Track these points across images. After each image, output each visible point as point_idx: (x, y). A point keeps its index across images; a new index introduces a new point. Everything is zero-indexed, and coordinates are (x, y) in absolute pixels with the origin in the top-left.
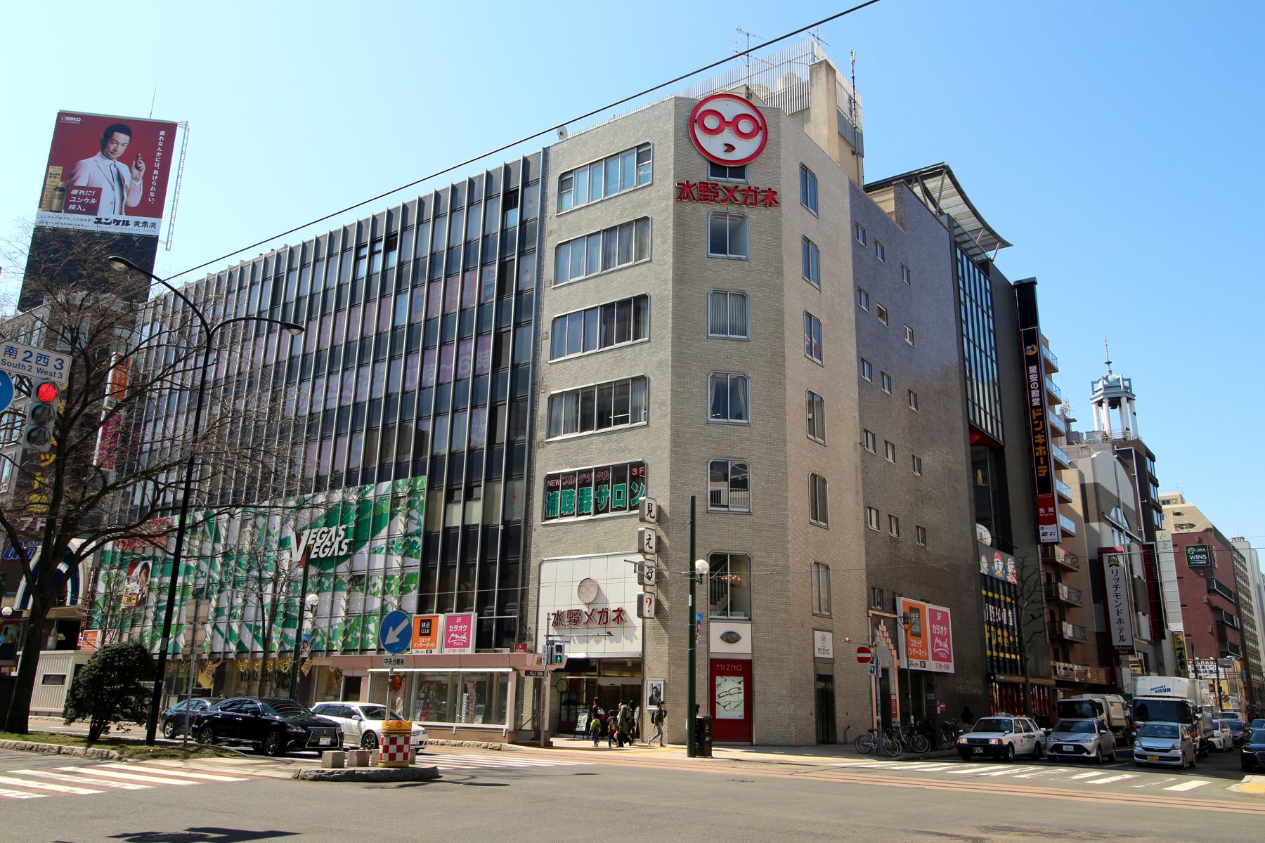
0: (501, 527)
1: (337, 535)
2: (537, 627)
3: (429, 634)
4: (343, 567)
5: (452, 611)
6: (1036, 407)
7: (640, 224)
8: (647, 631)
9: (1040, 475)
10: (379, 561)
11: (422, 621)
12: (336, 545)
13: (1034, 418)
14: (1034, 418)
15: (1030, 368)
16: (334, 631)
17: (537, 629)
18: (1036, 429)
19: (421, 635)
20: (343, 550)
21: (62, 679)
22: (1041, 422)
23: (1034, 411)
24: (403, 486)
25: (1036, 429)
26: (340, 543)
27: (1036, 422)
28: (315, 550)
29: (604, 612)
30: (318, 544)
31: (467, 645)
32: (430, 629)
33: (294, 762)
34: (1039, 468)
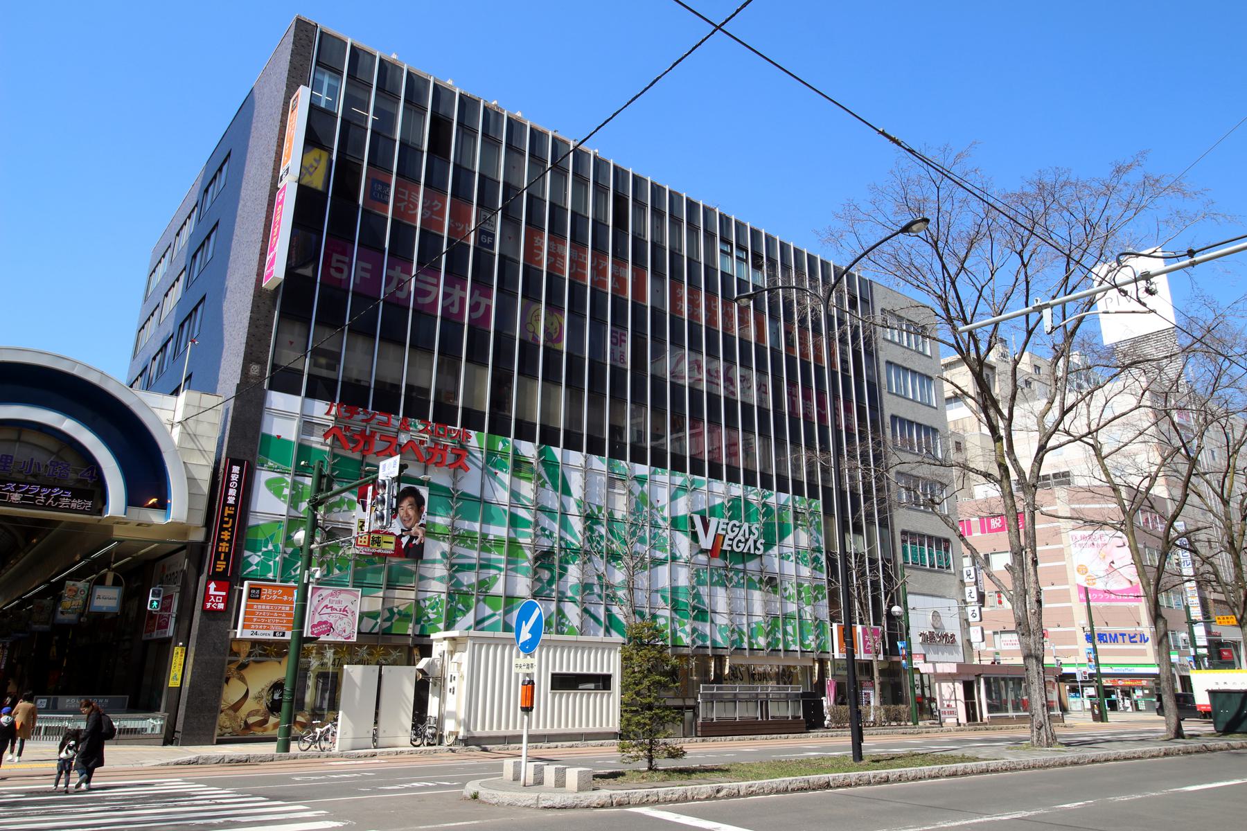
1: (751, 532)
4: (752, 565)
6: (230, 505)
9: (217, 570)
12: (751, 542)
13: (226, 515)
14: (226, 515)
15: (234, 467)
16: (752, 629)
18: (225, 526)
20: (759, 550)
22: (231, 520)
23: (227, 508)
25: (225, 526)
26: (755, 542)
27: (226, 519)
28: (727, 542)
29: (946, 635)
30: (731, 535)
34: (218, 562)
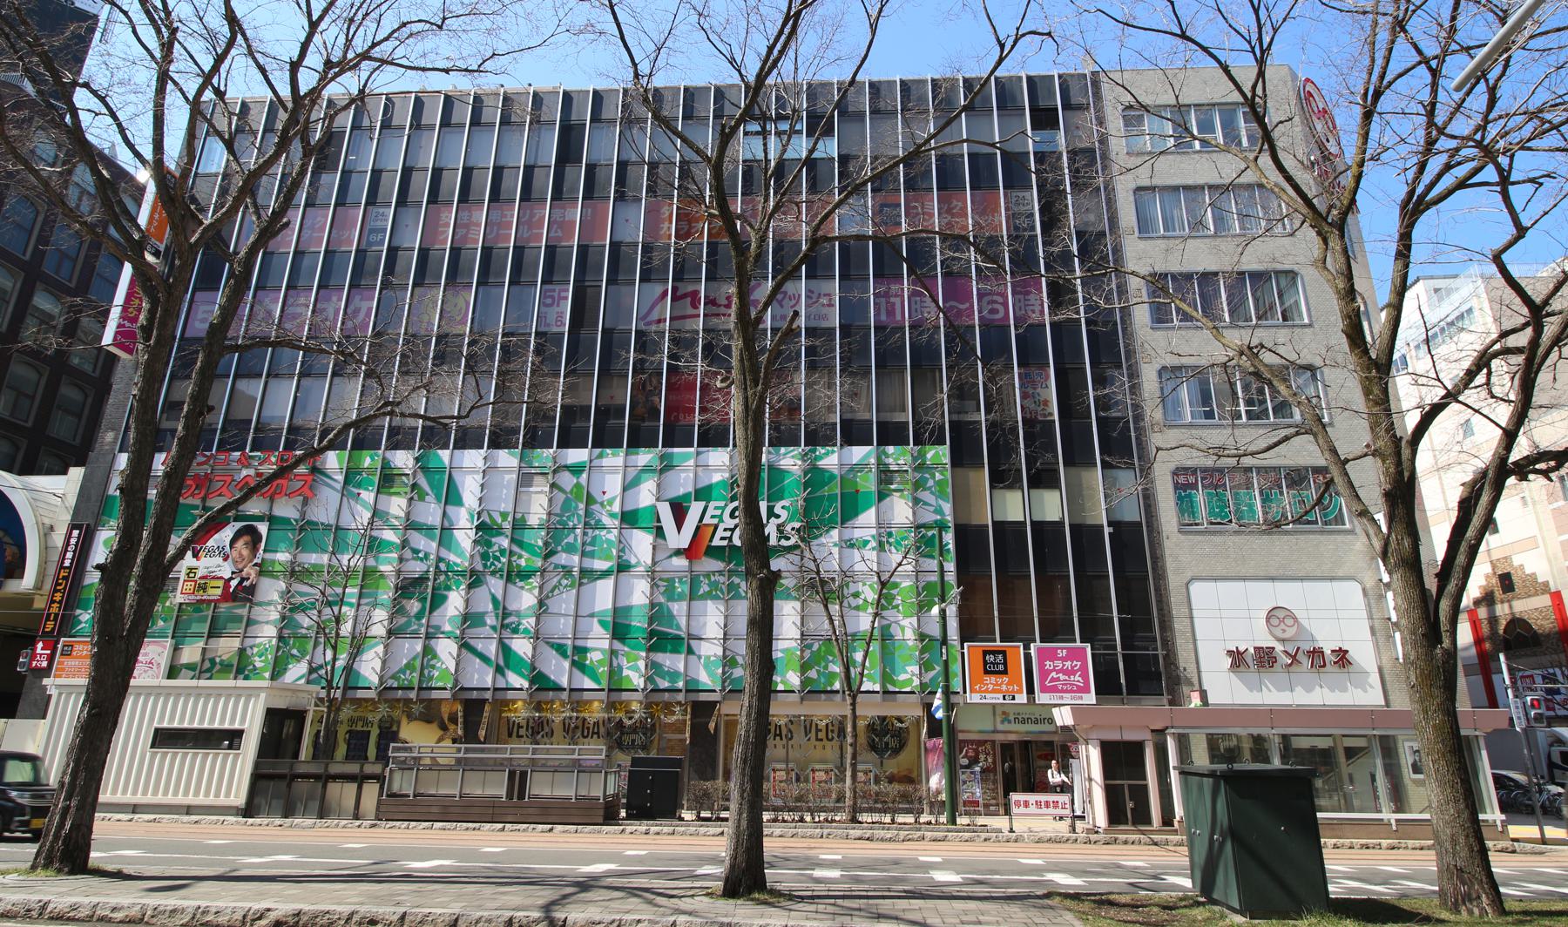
0: (1107, 530)
2: (1198, 668)
3: (1005, 672)
5: (1075, 641)
7: (1192, 195)
8: (1387, 678)
10: (865, 561)
11: (985, 653)
17: (1199, 672)
19: (986, 672)
21: (233, 738)
24: (897, 456)
31: (1086, 690)
32: (1005, 664)
33: (1556, 851)
